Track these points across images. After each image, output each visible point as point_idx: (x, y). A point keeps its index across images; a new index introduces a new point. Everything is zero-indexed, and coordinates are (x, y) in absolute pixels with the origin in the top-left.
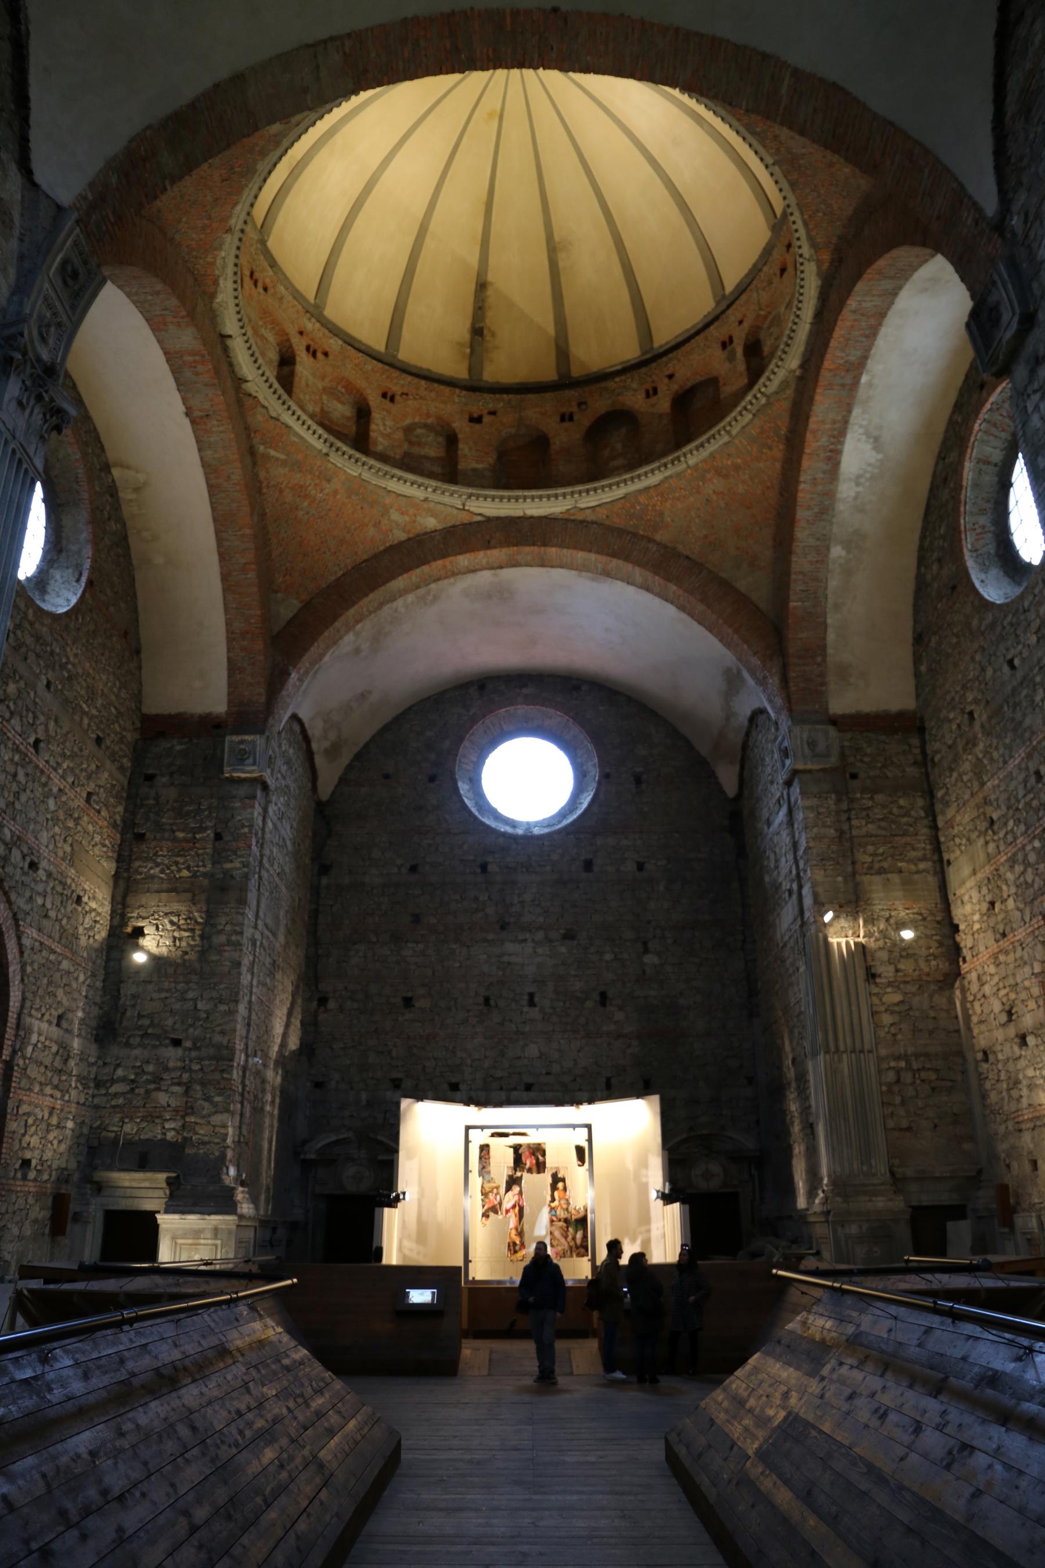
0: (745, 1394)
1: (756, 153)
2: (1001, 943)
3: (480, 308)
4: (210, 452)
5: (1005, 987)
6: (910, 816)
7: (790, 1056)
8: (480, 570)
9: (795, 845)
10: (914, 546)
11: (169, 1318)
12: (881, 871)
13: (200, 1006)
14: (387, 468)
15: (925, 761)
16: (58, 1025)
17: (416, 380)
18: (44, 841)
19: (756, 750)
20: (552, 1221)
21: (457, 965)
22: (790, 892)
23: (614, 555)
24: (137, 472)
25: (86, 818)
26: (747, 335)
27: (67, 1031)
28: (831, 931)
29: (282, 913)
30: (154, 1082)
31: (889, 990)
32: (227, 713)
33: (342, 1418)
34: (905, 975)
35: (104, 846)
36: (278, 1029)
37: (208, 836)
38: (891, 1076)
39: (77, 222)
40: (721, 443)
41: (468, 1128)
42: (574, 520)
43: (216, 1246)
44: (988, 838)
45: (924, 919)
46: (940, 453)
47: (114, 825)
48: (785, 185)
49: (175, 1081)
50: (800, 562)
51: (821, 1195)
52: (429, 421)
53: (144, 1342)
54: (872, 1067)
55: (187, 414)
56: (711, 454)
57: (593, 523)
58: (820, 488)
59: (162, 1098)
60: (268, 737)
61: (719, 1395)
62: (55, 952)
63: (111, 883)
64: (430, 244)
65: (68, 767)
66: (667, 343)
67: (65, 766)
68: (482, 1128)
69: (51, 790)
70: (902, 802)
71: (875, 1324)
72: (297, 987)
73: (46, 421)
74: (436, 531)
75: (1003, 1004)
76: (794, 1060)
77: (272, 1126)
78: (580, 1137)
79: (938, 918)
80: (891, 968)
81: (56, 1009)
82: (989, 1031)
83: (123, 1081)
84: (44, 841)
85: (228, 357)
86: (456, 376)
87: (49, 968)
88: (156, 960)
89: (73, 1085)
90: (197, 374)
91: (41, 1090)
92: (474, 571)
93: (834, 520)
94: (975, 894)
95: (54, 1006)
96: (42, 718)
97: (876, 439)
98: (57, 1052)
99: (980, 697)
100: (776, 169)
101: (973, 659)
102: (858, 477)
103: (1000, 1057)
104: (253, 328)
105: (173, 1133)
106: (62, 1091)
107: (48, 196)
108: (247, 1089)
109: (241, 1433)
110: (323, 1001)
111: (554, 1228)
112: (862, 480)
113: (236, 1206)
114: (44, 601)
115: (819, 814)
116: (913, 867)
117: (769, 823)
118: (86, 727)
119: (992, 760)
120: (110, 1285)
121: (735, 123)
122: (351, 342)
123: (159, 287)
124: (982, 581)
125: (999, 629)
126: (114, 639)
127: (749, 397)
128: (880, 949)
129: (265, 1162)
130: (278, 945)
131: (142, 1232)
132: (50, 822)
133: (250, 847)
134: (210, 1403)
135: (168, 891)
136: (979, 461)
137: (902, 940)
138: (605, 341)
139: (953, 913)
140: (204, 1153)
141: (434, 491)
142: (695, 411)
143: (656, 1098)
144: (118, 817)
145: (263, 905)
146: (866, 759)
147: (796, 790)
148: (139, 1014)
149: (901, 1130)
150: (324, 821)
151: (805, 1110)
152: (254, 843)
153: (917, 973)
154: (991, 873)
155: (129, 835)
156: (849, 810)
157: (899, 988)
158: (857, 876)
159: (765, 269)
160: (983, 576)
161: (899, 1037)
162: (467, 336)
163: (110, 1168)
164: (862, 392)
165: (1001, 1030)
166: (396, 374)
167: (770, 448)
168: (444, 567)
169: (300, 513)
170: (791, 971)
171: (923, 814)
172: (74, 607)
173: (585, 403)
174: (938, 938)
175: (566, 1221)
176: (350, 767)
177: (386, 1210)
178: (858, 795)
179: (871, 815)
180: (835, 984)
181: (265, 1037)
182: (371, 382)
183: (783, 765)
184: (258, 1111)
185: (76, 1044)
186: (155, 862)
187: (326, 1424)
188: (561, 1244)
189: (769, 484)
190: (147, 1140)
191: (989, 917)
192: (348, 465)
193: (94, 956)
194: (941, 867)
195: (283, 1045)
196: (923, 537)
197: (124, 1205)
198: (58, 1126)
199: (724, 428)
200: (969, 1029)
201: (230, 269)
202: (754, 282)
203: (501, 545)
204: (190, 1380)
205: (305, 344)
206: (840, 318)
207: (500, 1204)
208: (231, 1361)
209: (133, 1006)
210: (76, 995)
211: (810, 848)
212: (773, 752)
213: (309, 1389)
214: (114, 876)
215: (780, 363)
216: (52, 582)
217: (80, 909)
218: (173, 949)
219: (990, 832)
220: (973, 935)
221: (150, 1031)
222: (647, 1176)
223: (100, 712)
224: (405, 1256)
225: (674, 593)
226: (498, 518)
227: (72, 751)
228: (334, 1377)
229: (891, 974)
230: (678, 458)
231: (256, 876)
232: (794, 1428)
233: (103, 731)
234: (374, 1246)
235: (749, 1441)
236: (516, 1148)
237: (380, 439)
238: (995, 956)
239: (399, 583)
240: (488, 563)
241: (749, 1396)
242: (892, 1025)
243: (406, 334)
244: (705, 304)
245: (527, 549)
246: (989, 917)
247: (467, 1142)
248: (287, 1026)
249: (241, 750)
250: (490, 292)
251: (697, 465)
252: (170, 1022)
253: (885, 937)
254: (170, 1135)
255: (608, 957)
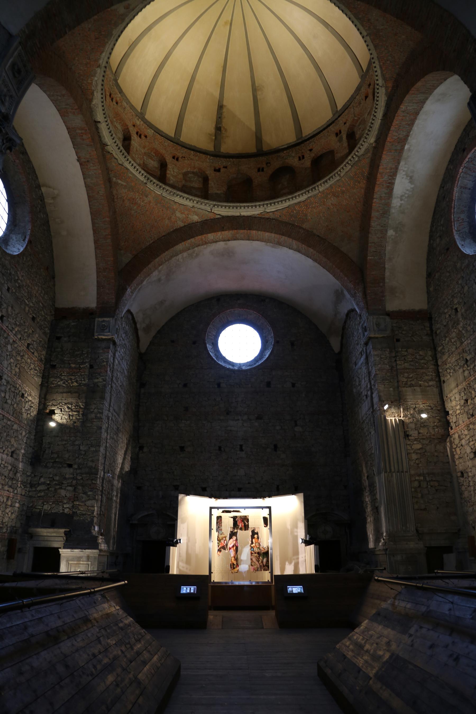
0: (363, 642)
1: (358, 30)
2: (471, 419)
3: (220, 118)
4: (89, 180)
5: (473, 441)
6: (425, 360)
7: (366, 475)
8: (219, 241)
9: (369, 373)
10: (428, 230)
11: (57, 602)
12: (411, 386)
13: (81, 448)
14: (175, 191)
15: (432, 333)
16: (12, 456)
17: (189, 151)
18: (5, 365)
19: (349, 329)
20: (252, 553)
21: (206, 431)
22: (367, 396)
23: (283, 234)
24: (54, 189)
25: (26, 356)
26: (348, 129)
27: (16, 459)
28: (387, 414)
29: (122, 405)
30: (59, 485)
31: (415, 442)
32: (96, 307)
33: (150, 654)
34: (423, 435)
35: (36, 370)
36: (120, 460)
37: (87, 366)
38: (416, 484)
39: (20, 43)
40: (335, 180)
41: (211, 508)
42: (264, 218)
43: (88, 565)
44: (465, 369)
45: (432, 409)
46: (441, 185)
47: (41, 360)
48: (372, 47)
49: (69, 484)
50: (373, 238)
51: (383, 541)
52: (195, 170)
53: (40, 616)
54: (407, 479)
55: (78, 160)
56: (330, 185)
57: (273, 219)
58: (383, 201)
59: (63, 493)
60: (116, 319)
61: (347, 642)
62: (10, 420)
63: (39, 389)
64: (196, 86)
65: (18, 330)
66: (309, 134)
67: (16, 329)
68: (218, 508)
69: (9, 341)
70: (421, 353)
71: (442, 605)
72: (129, 441)
73: (3, 144)
74: (198, 222)
75: (472, 449)
76: (368, 477)
77: (116, 507)
78: (265, 513)
79: (439, 408)
80: (416, 432)
81: (11, 449)
82: (464, 462)
83: (44, 484)
84: (5, 365)
85: (98, 133)
86: (208, 150)
87: (7, 428)
88: (59, 424)
89: (19, 486)
90: (83, 140)
91: (3, 488)
92: (216, 242)
93: (390, 217)
94: (457, 396)
95: (10, 447)
96: (5, 305)
97: (411, 178)
98: (11, 470)
99: (461, 301)
100: (368, 38)
101: (457, 282)
102: (402, 196)
103: (470, 474)
104: (111, 121)
105: (68, 509)
106: (13, 488)
107: (4, 28)
108: (104, 489)
109: (95, 667)
110: (141, 448)
111: (252, 557)
112: (404, 198)
113: (98, 545)
114: (7, 249)
115: (381, 358)
116: (426, 384)
117: (356, 364)
118: (27, 311)
119: (467, 331)
120: (31, 584)
121: (349, 13)
122: (158, 131)
123: (64, 92)
124: (462, 245)
125: (471, 267)
126: (42, 270)
127: (350, 158)
128: (411, 422)
129: (113, 525)
130: (120, 420)
131: (53, 558)
132: (8, 357)
133: (107, 371)
134: (77, 650)
135: (66, 392)
136: (461, 187)
137: (422, 418)
138: (280, 134)
139: (446, 406)
140: (83, 519)
141: (197, 203)
142: (323, 166)
143: (301, 495)
144: (43, 357)
145: (112, 400)
146: (404, 332)
147: (370, 346)
148: (52, 452)
149: (421, 510)
150: (142, 362)
151: (374, 500)
152: (109, 370)
153: (429, 434)
154: (466, 385)
155: (48, 366)
156: (396, 356)
157: (420, 442)
158: (400, 388)
159: (358, 97)
160: (463, 243)
161: (420, 465)
162: (213, 131)
163: (37, 527)
164: (405, 154)
165: (470, 462)
166: (179, 147)
167: (359, 182)
168: (202, 239)
169: (133, 212)
170: (367, 434)
171: (431, 358)
172: (21, 252)
173: (270, 163)
174: (438, 418)
175: (258, 553)
176: (155, 337)
177: (171, 548)
178: (400, 350)
179: (406, 358)
180: (389, 439)
181: (113, 464)
182: (168, 151)
183: (364, 335)
184: (110, 499)
185: (21, 465)
186: (60, 378)
187: (142, 659)
188: (255, 564)
189: (358, 200)
190: (55, 513)
191: (465, 407)
192: (156, 190)
193: (30, 423)
194: (440, 384)
195: (122, 468)
196: (432, 226)
197: (43, 544)
198: (11, 506)
199: (337, 173)
200: (454, 461)
201: (99, 87)
202: (352, 104)
203: (229, 229)
204: (66, 637)
205: (136, 131)
206: (397, 115)
207: (227, 545)
208: (90, 626)
209: (49, 448)
210: (21, 442)
211: (377, 374)
212: (358, 330)
213: (133, 640)
214: (40, 385)
215: (365, 140)
216: (11, 240)
217: (23, 400)
218: (69, 420)
219: (466, 366)
220: (456, 416)
221: (57, 460)
222: (297, 532)
223: (34, 305)
224: (180, 570)
225: (312, 253)
226: (228, 217)
227: (20, 323)
228: (146, 632)
229: (416, 435)
230: (315, 188)
231: (110, 386)
232: (396, 663)
233: (36, 315)
234: (166, 565)
235: (369, 669)
236: (235, 518)
237: (171, 178)
238: (468, 426)
239: (180, 247)
240: (222, 238)
241: (365, 643)
242: (416, 459)
243: (184, 129)
244: (328, 115)
245: (242, 231)
246: (465, 407)
247: (211, 515)
248: (124, 459)
249: (103, 325)
250: (224, 110)
251: (324, 191)
252: (67, 456)
253: (413, 417)
254: (66, 511)
255: (278, 428)
